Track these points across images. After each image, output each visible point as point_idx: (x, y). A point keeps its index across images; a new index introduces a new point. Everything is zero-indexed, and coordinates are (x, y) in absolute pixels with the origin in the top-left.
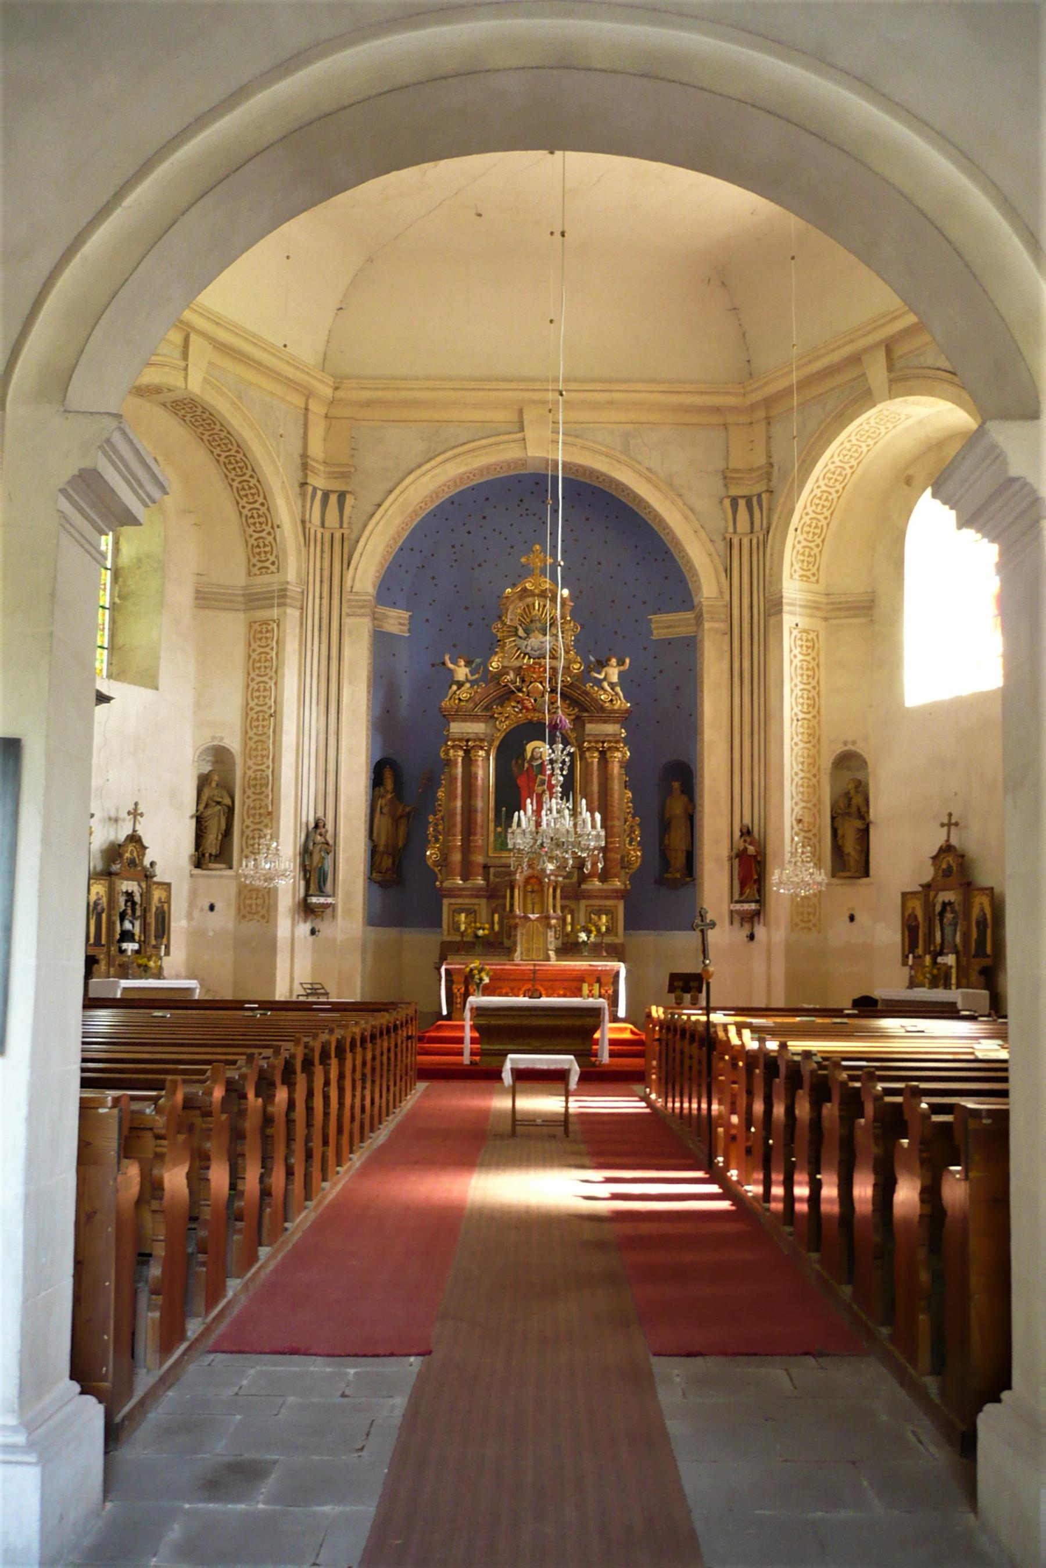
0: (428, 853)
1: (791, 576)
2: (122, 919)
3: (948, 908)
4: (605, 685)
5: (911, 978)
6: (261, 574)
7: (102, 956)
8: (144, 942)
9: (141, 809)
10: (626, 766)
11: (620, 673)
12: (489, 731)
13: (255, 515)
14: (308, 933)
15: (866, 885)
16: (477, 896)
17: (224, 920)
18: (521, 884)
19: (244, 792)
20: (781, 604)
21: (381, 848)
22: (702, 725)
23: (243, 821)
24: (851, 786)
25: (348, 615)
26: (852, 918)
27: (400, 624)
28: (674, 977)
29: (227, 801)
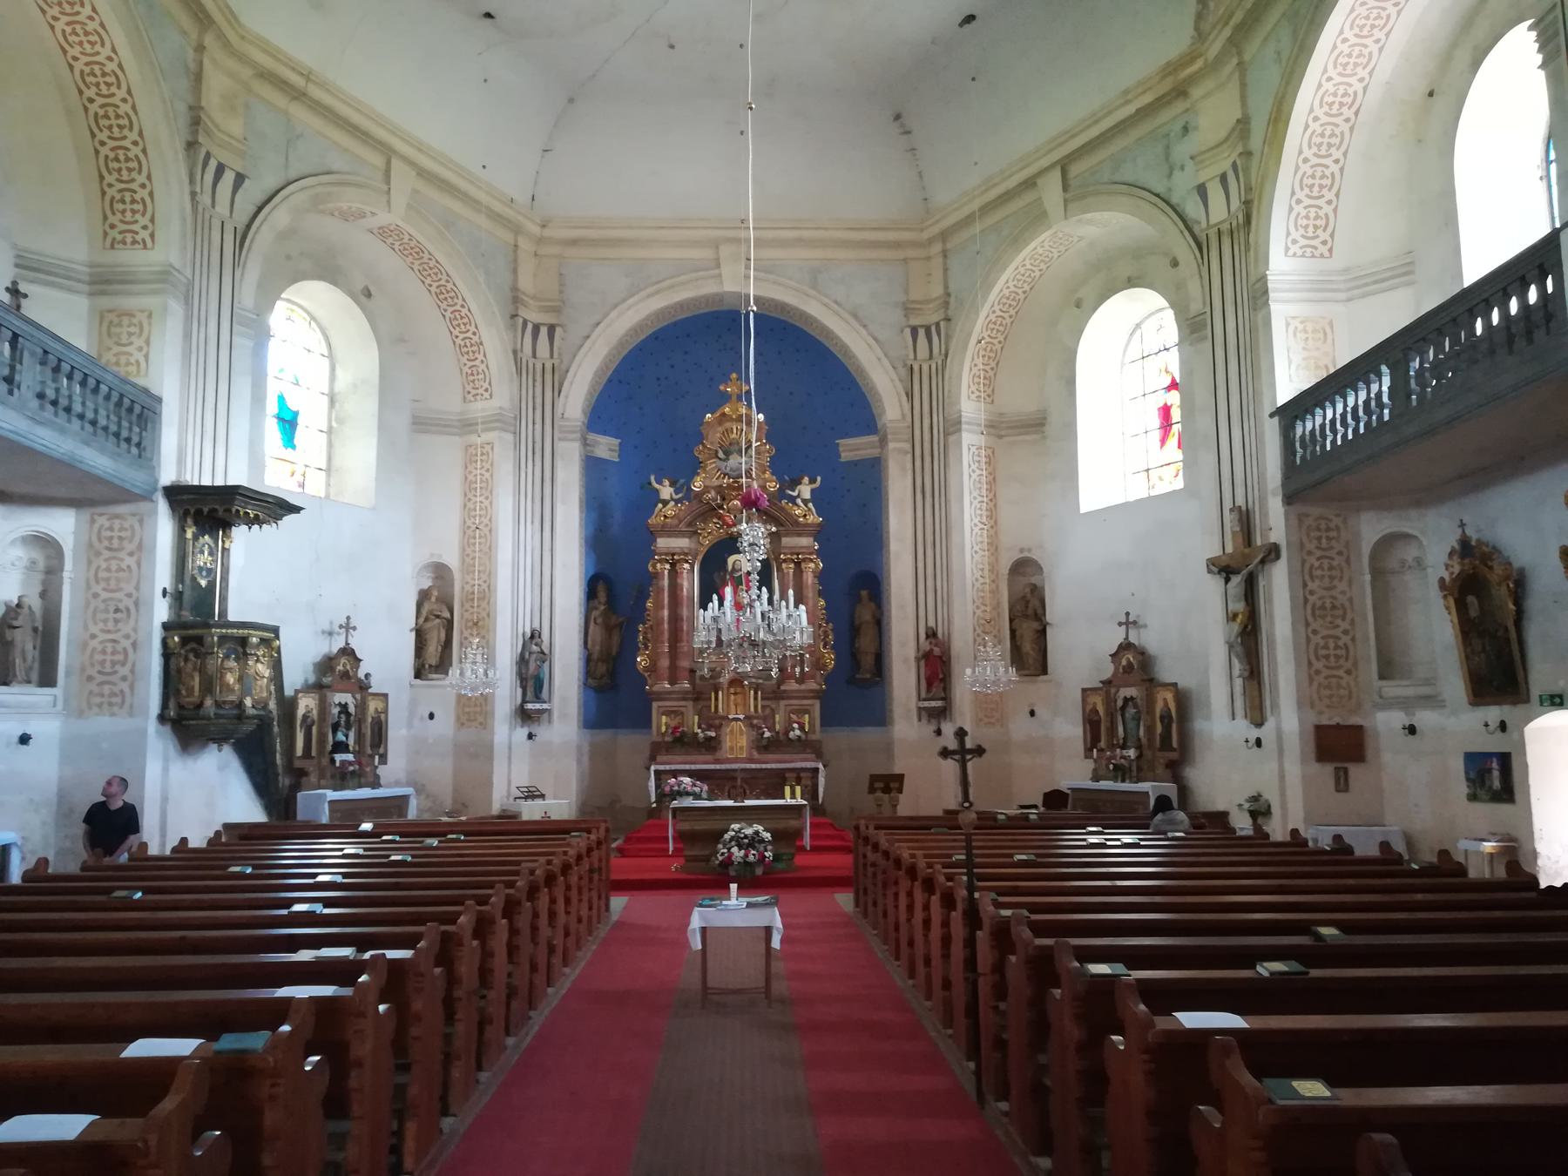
0: (639, 660)
1: (969, 397)
2: (335, 731)
3: (1130, 703)
4: (799, 501)
5: (1095, 770)
6: (476, 400)
7: (311, 769)
8: (359, 752)
9: (353, 623)
10: (821, 576)
11: (813, 491)
12: (693, 546)
13: (468, 345)
14: (526, 737)
15: (1045, 681)
16: (684, 699)
17: (445, 725)
18: (726, 686)
19: (462, 606)
20: (960, 422)
21: (595, 656)
22: (888, 538)
23: (462, 633)
24: (1028, 590)
25: (560, 439)
26: (1032, 713)
27: (610, 450)
28: (874, 778)
29: (447, 615)
